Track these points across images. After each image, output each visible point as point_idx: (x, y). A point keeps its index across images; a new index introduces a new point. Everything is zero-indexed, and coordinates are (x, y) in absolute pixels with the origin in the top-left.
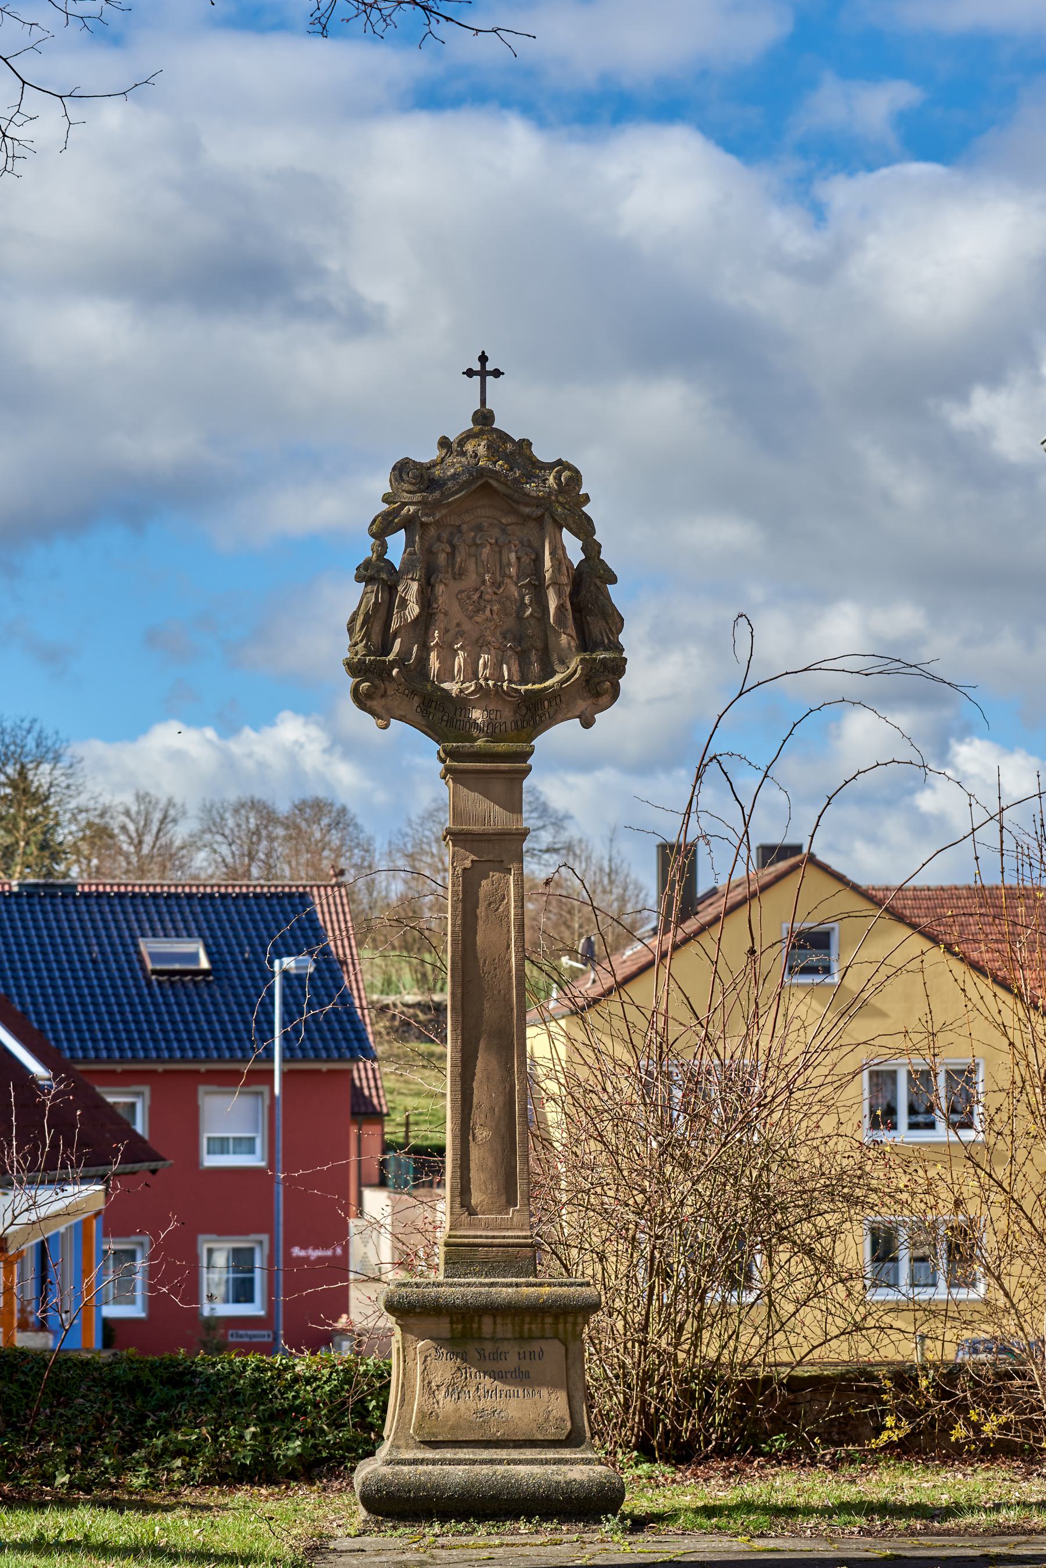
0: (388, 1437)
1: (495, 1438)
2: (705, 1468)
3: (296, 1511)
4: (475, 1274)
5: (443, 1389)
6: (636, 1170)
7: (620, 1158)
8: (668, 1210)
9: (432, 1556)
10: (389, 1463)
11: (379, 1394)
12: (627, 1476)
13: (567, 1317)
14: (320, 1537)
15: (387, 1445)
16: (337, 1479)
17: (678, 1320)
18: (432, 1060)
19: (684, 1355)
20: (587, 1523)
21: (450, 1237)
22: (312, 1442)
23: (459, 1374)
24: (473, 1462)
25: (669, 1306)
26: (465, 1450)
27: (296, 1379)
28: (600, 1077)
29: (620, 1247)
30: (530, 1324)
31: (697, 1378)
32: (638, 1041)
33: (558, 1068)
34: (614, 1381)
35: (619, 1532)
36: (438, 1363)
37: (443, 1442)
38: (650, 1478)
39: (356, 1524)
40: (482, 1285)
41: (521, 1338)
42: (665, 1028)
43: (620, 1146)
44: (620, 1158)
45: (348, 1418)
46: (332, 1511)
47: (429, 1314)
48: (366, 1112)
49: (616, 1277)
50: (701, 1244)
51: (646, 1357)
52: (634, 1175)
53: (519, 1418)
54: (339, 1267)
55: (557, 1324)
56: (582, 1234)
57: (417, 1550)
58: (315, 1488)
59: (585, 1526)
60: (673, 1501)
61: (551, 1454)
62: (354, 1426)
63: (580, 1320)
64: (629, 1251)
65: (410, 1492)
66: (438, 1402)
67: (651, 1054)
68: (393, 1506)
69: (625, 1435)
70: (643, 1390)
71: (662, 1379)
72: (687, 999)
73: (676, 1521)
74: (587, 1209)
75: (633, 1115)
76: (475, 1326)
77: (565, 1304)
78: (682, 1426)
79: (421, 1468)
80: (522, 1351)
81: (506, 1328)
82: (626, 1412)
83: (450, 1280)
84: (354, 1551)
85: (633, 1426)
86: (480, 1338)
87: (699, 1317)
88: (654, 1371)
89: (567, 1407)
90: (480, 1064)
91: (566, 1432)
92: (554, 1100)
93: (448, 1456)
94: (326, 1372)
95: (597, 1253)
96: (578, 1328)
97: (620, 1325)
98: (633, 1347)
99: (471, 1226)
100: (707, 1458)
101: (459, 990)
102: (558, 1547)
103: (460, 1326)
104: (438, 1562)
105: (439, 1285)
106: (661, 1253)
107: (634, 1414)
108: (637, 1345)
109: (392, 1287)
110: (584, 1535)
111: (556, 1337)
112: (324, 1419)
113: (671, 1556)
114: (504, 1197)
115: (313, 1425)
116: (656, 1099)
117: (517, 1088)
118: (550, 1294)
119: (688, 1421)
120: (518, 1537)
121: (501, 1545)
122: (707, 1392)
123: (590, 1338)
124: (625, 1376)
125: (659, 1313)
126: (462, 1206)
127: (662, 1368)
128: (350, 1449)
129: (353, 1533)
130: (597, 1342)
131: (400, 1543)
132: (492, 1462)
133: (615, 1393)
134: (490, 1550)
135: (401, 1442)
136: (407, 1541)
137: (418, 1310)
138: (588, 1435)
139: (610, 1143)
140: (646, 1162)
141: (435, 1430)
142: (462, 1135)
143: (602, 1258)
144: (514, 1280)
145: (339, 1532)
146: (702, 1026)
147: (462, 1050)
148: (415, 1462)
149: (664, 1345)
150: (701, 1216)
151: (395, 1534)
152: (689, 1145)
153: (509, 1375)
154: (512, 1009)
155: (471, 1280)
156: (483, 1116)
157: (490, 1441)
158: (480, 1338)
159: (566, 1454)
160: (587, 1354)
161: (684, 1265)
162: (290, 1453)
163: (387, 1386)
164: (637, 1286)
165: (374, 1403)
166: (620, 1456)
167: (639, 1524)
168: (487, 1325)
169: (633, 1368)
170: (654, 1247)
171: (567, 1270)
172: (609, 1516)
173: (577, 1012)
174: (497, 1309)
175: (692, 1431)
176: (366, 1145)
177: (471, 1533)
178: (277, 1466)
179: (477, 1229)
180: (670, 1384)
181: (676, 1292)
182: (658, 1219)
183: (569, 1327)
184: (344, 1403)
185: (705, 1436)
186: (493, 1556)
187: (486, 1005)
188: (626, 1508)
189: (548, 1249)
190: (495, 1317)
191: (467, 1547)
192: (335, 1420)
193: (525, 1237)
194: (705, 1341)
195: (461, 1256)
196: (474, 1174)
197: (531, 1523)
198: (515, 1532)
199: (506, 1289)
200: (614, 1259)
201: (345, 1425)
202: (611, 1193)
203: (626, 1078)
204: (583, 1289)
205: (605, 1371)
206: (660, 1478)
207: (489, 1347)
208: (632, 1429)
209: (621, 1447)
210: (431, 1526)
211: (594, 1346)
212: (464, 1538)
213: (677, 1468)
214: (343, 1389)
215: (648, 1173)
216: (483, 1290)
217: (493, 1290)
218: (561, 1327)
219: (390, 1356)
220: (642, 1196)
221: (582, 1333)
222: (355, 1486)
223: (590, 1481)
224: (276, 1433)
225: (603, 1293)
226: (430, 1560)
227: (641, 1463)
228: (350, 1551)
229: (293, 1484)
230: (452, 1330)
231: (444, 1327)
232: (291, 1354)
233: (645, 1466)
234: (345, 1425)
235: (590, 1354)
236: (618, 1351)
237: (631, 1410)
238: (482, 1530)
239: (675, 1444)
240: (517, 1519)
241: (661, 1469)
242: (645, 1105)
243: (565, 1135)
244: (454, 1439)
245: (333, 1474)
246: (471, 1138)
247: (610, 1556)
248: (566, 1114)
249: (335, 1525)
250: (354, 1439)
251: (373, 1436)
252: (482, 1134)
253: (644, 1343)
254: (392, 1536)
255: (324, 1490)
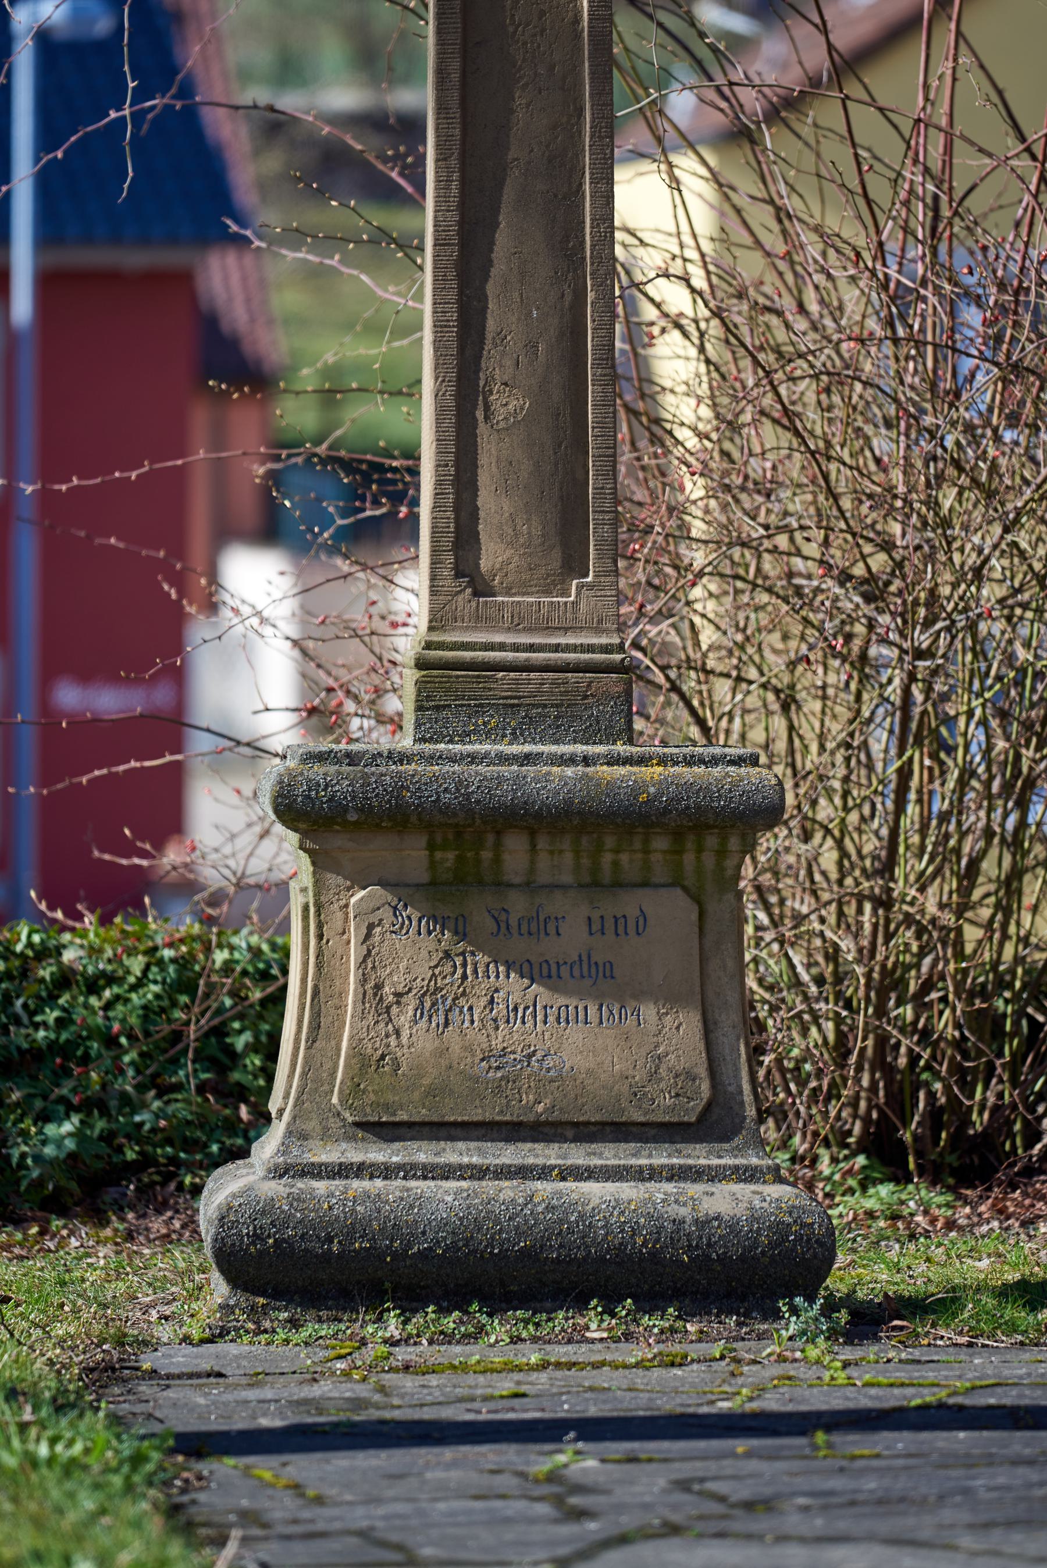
0: (281, 1112)
1: (532, 1118)
2: (1025, 1195)
3: (63, 1283)
4: (487, 735)
5: (411, 1003)
6: (870, 496)
7: (833, 467)
8: (946, 591)
9: (382, 1389)
10: (279, 1172)
11: (260, 1017)
12: (842, 1211)
13: (702, 837)
14: (120, 1341)
15: (277, 1132)
16: (159, 1212)
17: (966, 849)
18: (394, 248)
19: (979, 933)
20: (745, 1317)
21: (429, 646)
22: (100, 1125)
23: (448, 968)
24: (479, 1173)
25: (944, 817)
26: (461, 1145)
27: (65, 979)
28: (790, 278)
29: (832, 679)
30: (617, 851)
31: (1010, 986)
32: (879, 190)
33: (692, 254)
34: (813, 989)
35: (820, 1340)
36: (399, 942)
37: (410, 1125)
38: (895, 1217)
39: (204, 1313)
40: (504, 759)
41: (593, 884)
42: (948, 162)
43: (835, 441)
44: (833, 467)
45: (188, 1073)
46: (153, 1288)
47: (378, 826)
48: (237, 370)
49: (822, 748)
50: (1022, 671)
51: (889, 937)
52: (864, 509)
53: (589, 1072)
54: (170, 727)
55: (680, 852)
56: (742, 647)
57: (346, 1374)
58: (108, 1232)
59: (739, 1324)
60: (948, 1271)
61: (661, 1157)
62: (201, 1089)
63: (734, 843)
64: (853, 686)
65: (330, 1239)
66: (398, 1033)
67: (912, 223)
68: (289, 1272)
69: (838, 1117)
70: (881, 1011)
71: (927, 986)
72: (1000, 93)
73: (954, 1315)
74: (755, 586)
75: (868, 367)
76: (486, 855)
77: (698, 807)
78: (971, 1097)
79: (357, 1185)
80: (595, 915)
81: (558, 862)
82: (841, 1062)
83: (428, 748)
84: (198, 1375)
85: (857, 1097)
86: (498, 884)
87: (1015, 843)
88: (907, 968)
89: (702, 1046)
90: (503, 241)
91: (697, 1105)
92: (678, 326)
93: (422, 1158)
94: (136, 964)
95: (777, 691)
96: (730, 863)
97: (829, 859)
98: (860, 911)
99: (480, 620)
100: (1030, 1171)
101: (455, 65)
102: (678, 1372)
103: (451, 855)
104: (396, 1401)
105: (403, 758)
106: (928, 690)
107: (859, 1069)
108: (868, 907)
109: (291, 763)
110: (738, 1345)
111: (677, 882)
112: (131, 1072)
113: (942, 1394)
114: (557, 554)
115: (104, 1086)
116: (922, 330)
117: (591, 296)
118: (663, 784)
119: (986, 1087)
120: (584, 1347)
121: (544, 1365)
122: (1031, 1020)
123: (759, 889)
124: (838, 979)
125: (923, 831)
126: (458, 574)
127: (927, 961)
128: (191, 1145)
129: (196, 1334)
130: (773, 899)
131: (306, 1359)
132: (523, 1172)
133: (816, 1019)
134: (517, 1376)
135: (312, 1125)
136: (322, 1354)
137: (352, 817)
138: (751, 1112)
139: (811, 433)
140: (897, 476)
141: (390, 1097)
142: (459, 408)
143: (788, 703)
144: (580, 748)
145: (165, 1332)
146: (1034, 158)
147: (462, 207)
148: (342, 1171)
149: (932, 909)
150: (1025, 606)
151: (296, 1338)
152: (997, 439)
153: (565, 971)
154: (581, 110)
155: (477, 747)
156: (508, 362)
157: (520, 1124)
158: (498, 884)
159: (700, 1156)
160: (749, 930)
161: (983, 722)
162: (49, 1151)
163: (279, 998)
164: (870, 767)
165: (247, 1037)
166: (825, 1166)
167: (866, 1321)
168: (515, 854)
169: (858, 961)
170: (912, 677)
171: (705, 729)
172: (798, 1300)
173: (740, 135)
174: (538, 815)
175: (996, 1109)
176: (227, 450)
177: (469, 1338)
178: (18, 1182)
179: (494, 629)
180: (944, 999)
181: (962, 783)
182: (922, 612)
183: (709, 860)
184: (177, 1036)
185: (1026, 1123)
186: (523, 1389)
187: (520, 100)
188: (837, 1283)
189: (660, 679)
190: (533, 834)
191: (464, 1368)
192: (156, 1075)
193: (606, 649)
194: (1029, 900)
195: (450, 686)
196: (487, 500)
197: (613, 1315)
198: (577, 1336)
199: (556, 767)
200: (817, 706)
201: (178, 1087)
202: (812, 549)
203: (853, 279)
204: (743, 770)
205: (792, 966)
206: (919, 1218)
207: (518, 905)
208: (854, 1103)
209: (827, 1144)
210: (379, 1319)
211: (767, 907)
212: (458, 1349)
213: (959, 1197)
214: (174, 1004)
215: (899, 503)
216: (506, 770)
217: (530, 770)
218: (689, 859)
219: (285, 928)
220: (882, 557)
221: (738, 877)
222: (203, 1229)
223: (753, 1219)
224: (18, 1104)
225: (788, 785)
226: (377, 1397)
227: (875, 1182)
228: (191, 1376)
229: (56, 1223)
230: (433, 864)
231: (413, 856)
232: (54, 921)
233: (884, 1190)
234: (178, 1087)
235: (758, 928)
236: (822, 920)
237: (853, 1059)
238: (498, 1330)
239: (955, 1139)
240: (581, 1305)
241: (920, 1198)
242: (896, 341)
243: (705, 412)
244: (435, 1118)
245: (152, 1200)
246: (480, 414)
247: (798, 1392)
248: (708, 362)
249: (154, 1315)
250: (202, 1122)
251: (244, 1112)
252: (507, 404)
253: (884, 902)
254: (287, 1341)
255: (130, 1236)
